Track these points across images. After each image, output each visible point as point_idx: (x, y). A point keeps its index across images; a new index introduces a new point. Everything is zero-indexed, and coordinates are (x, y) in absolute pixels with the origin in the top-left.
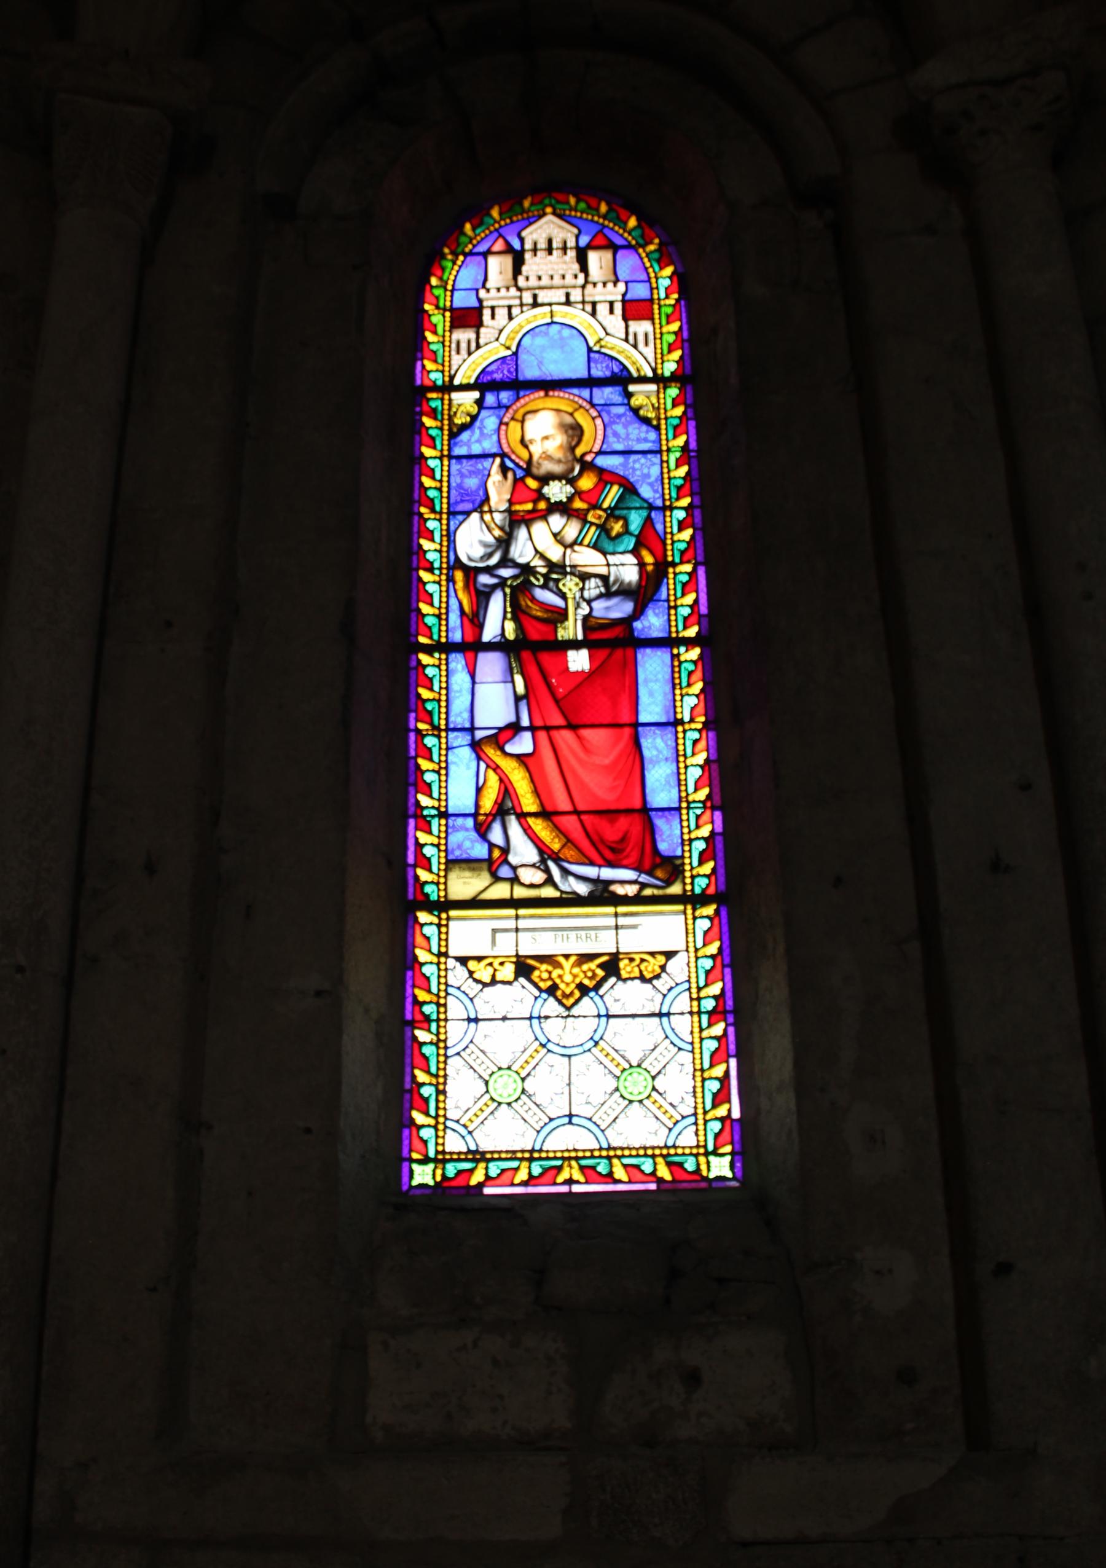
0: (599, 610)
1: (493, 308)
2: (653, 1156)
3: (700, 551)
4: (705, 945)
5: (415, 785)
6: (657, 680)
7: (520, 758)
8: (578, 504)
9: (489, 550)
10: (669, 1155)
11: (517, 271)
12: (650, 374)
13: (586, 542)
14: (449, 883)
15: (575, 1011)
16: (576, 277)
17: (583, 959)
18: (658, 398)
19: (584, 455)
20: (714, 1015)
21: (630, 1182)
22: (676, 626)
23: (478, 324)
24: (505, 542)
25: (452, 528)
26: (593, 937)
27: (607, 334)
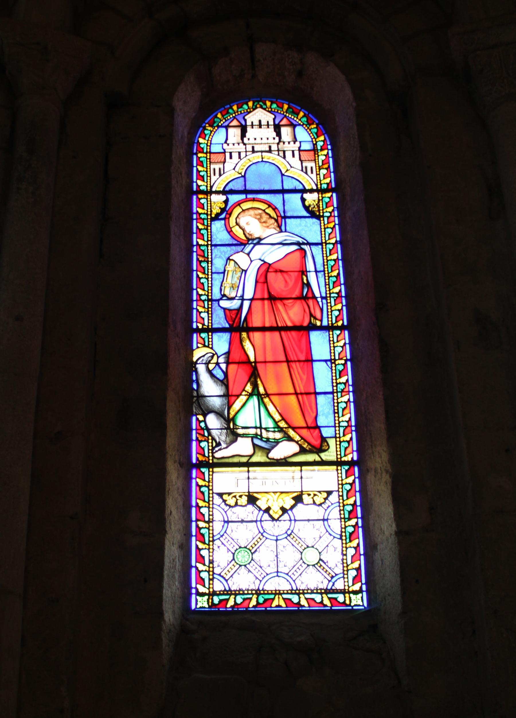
4: (352, 563)
11: (243, 134)
12: (315, 188)
16: (274, 139)
22: (326, 254)
27: (291, 167)
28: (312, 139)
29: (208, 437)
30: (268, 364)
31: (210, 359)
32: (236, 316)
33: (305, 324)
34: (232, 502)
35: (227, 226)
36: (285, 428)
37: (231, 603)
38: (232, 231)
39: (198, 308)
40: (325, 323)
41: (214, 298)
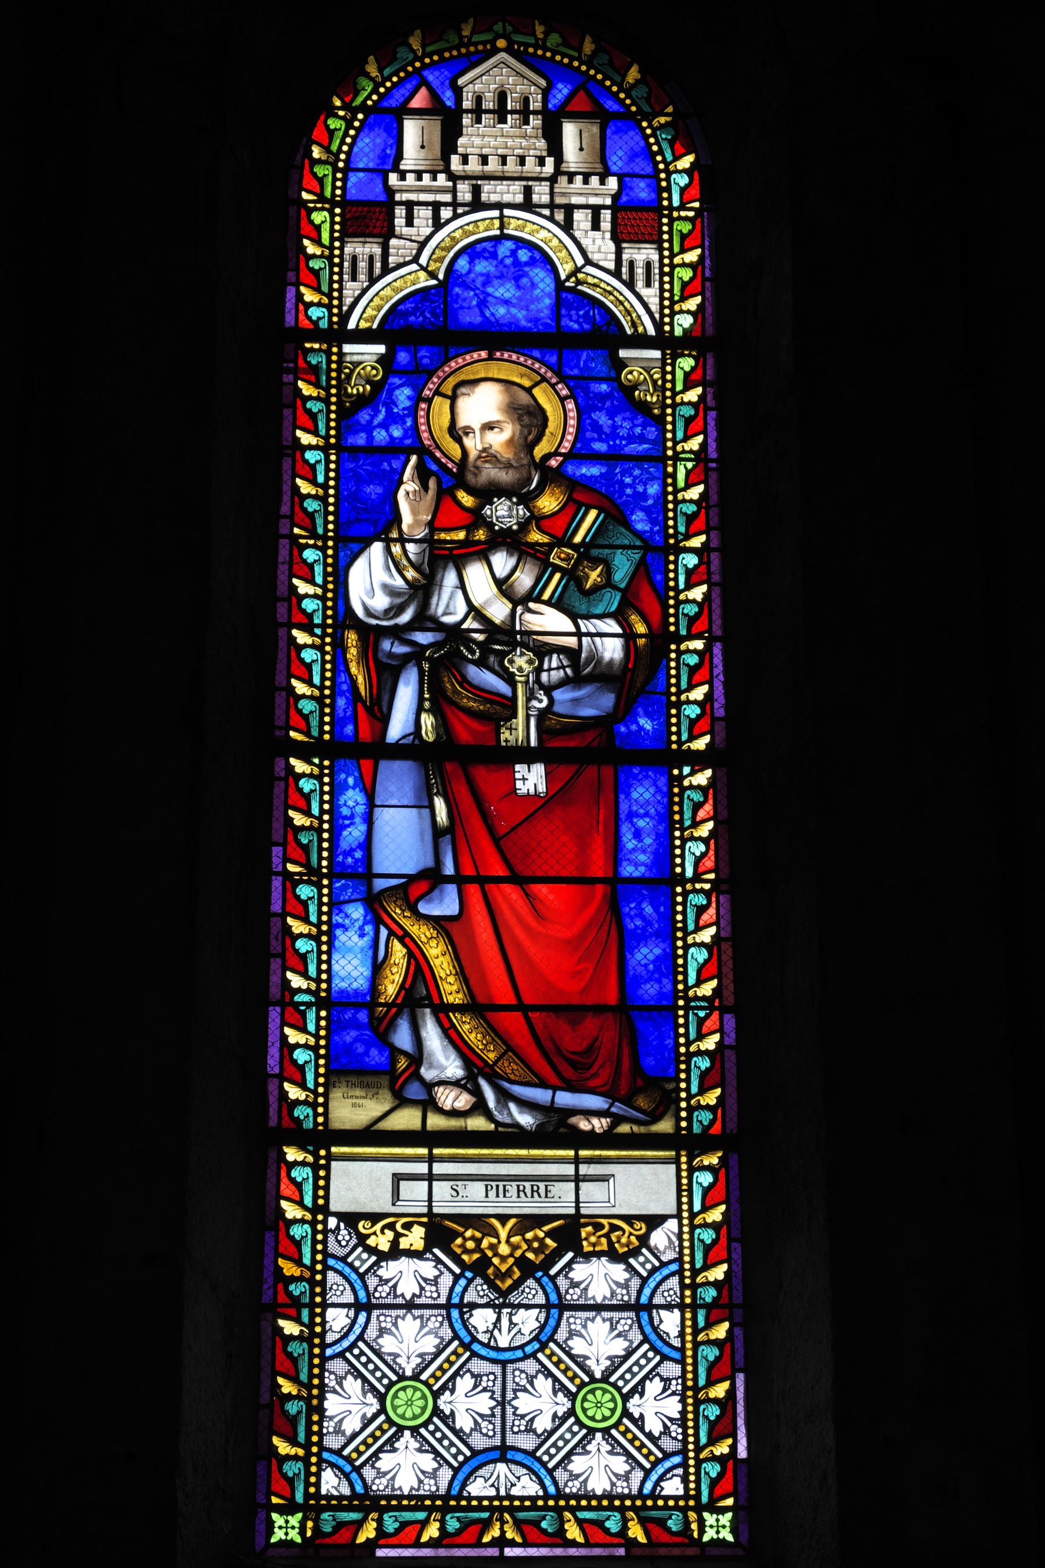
0: (564, 702)
1: (410, 205)
2: (622, 1510)
3: (717, 622)
5: (282, 956)
6: (647, 814)
7: (439, 923)
8: (535, 536)
9: (399, 601)
10: (645, 1506)
13: (546, 596)
14: (331, 1104)
15: (514, 1298)
16: (541, 162)
17: (527, 1223)
18: (664, 373)
19: (547, 457)
20: (715, 1313)
21: (587, 1544)
23: (387, 233)
24: (423, 590)
25: (342, 563)
26: (542, 1191)
34: (383, 1241)
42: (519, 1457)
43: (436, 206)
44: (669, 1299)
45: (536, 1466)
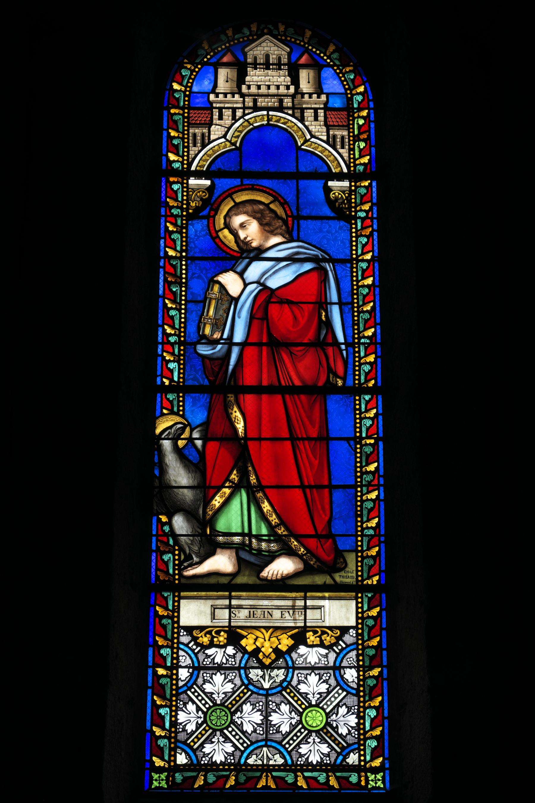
1: (220, 109)
16: (288, 88)
28: (346, 90)
29: (174, 547)
30: (263, 442)
31: (179, 432)
32: (220, 369)
33: (321, 384)
34: (205, 640)
35: (212, 228)
36: (285, 535)
37: (200, 782)
38: (218, 237)
39: (165, 354)
40: (350, 383)
41: (189, 340)
42: (274, 744)
43: (234, 110)
44: (350, 662)
45: (282, 750)
